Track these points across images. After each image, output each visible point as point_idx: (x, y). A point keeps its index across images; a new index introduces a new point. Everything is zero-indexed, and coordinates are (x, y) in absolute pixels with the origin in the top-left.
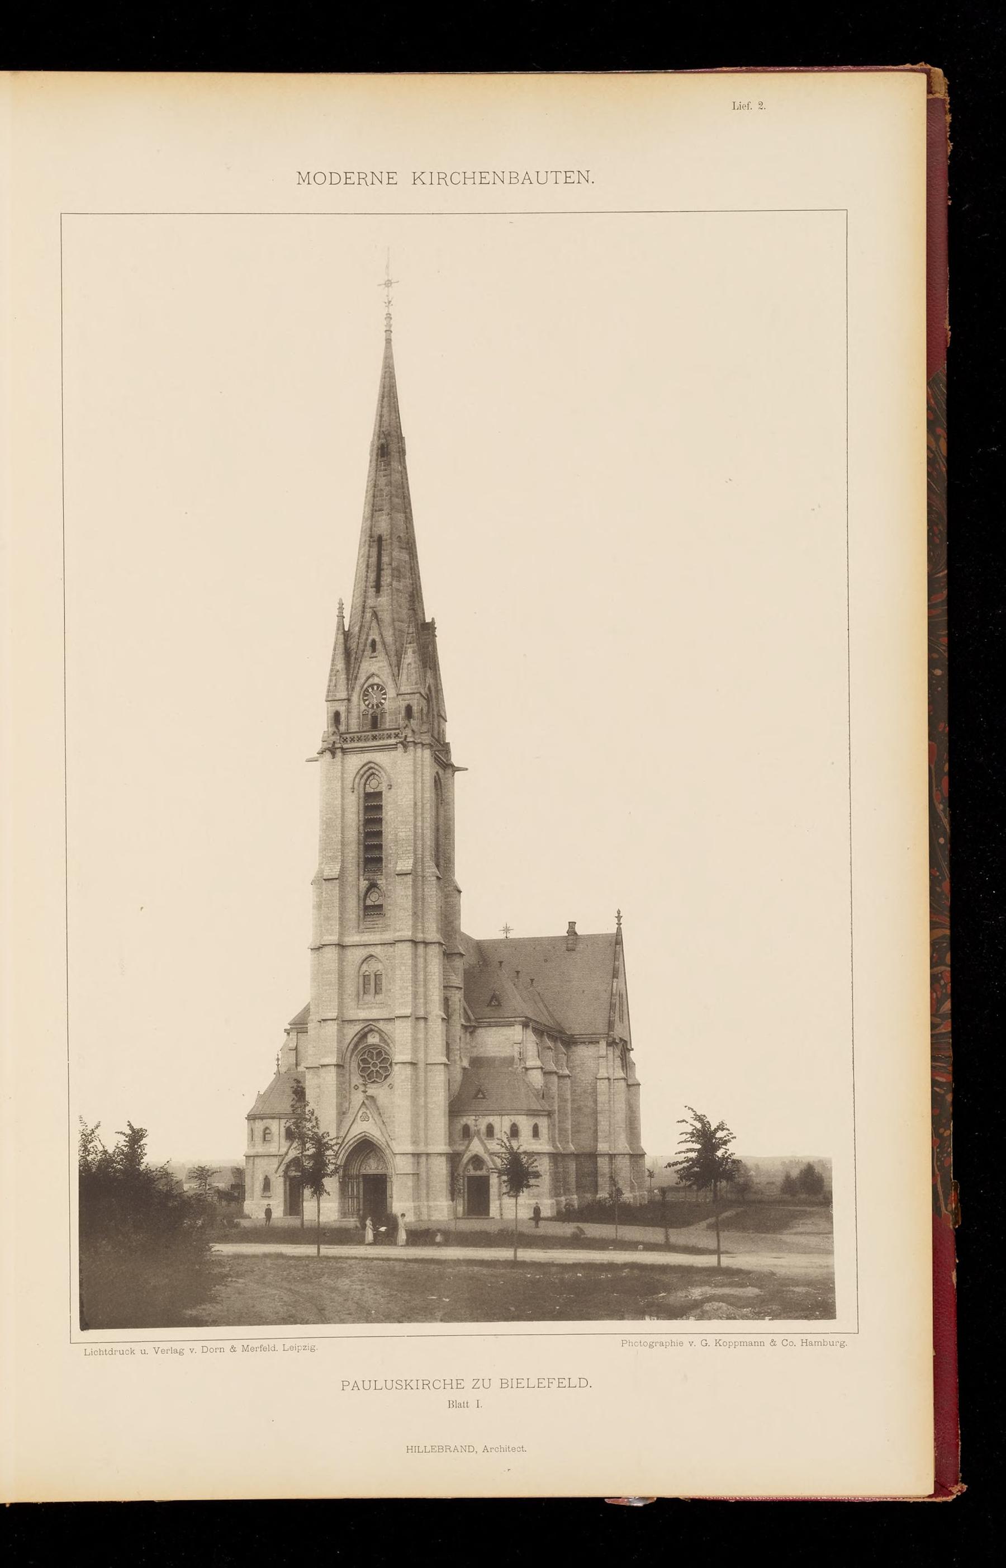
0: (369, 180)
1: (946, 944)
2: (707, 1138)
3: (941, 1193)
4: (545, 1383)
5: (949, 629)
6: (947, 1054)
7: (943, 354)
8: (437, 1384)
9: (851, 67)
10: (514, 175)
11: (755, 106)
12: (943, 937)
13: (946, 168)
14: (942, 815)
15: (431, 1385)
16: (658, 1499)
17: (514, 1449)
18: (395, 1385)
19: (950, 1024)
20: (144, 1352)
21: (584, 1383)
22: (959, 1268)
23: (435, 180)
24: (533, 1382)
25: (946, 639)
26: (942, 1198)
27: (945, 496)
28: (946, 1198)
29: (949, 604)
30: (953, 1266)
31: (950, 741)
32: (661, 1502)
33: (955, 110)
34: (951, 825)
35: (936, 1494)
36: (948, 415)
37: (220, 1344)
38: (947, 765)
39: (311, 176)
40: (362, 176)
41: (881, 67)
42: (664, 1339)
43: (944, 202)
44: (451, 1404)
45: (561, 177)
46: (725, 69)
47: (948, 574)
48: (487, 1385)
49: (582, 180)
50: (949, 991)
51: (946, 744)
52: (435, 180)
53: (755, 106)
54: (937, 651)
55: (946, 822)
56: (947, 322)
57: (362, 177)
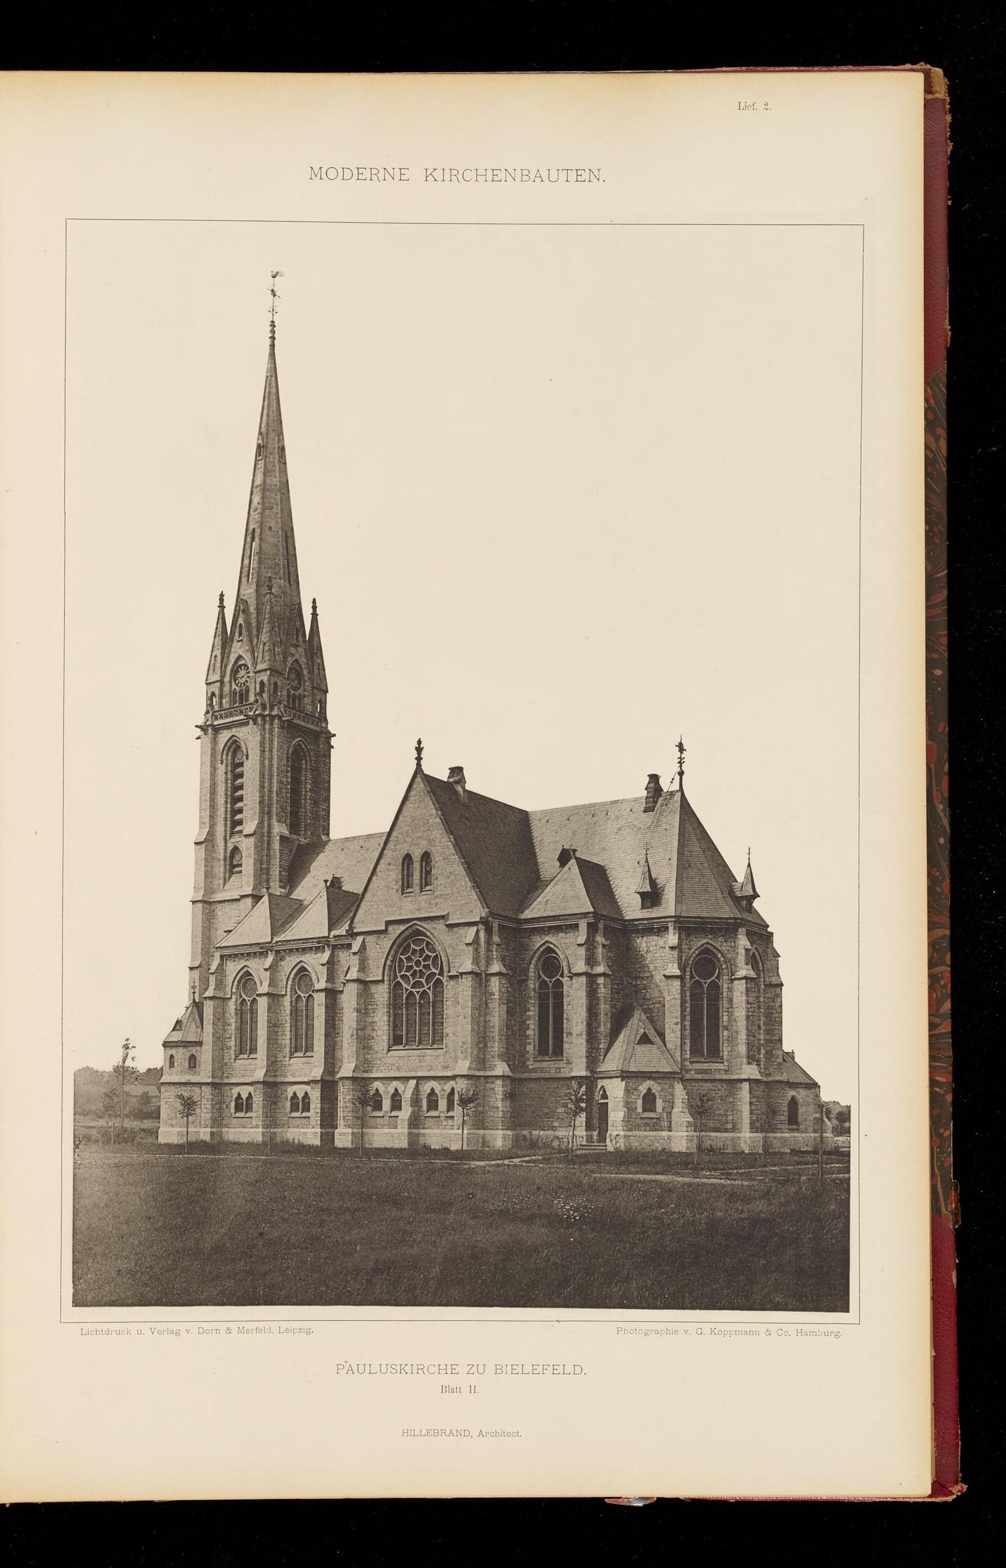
0: (381, 176)
1: (946, 944)
2: (457, 771)
3: (941, 1193)
4: (540, 1369)
6: (948, 1054)
7: (943, 354)
8: (432, 1369)
9: (851, 67)
10: (525, 173)
11: (760, 106)
13: (946, 168)
14: (942, 814)
15: (425, 1370)
16: (658, 1499)
17: (509, 1434)
20: (140, 1332)
21: (578, 1369)
23: (447, 177)
25: (946, 639)
26: (942, 1198)
27: (945, 496)
28: (946, 1199)
30: (952, 1266)
31: (950, 741)
32: (661, 1500)
33: (955, 109)
34: (951, 825)
35: (935, 1492)
36: (948, 415)
37: (215, 1326)
38: (947, 765)
39: (324, 171)
41: (882, 67)
42: (660, 1327)
43: (943, 201)
44: (444, 1389)
45: (572, 175)
46: (725, 69)
47: (948, 574)
48: (481, 1370)
50: (949, 991)
51: (946, 744)
52: (447, 177)
53: (760, 106)
54: (937, 651)
55: (946, 822)
56: (947, 322)
57: (374, 173)
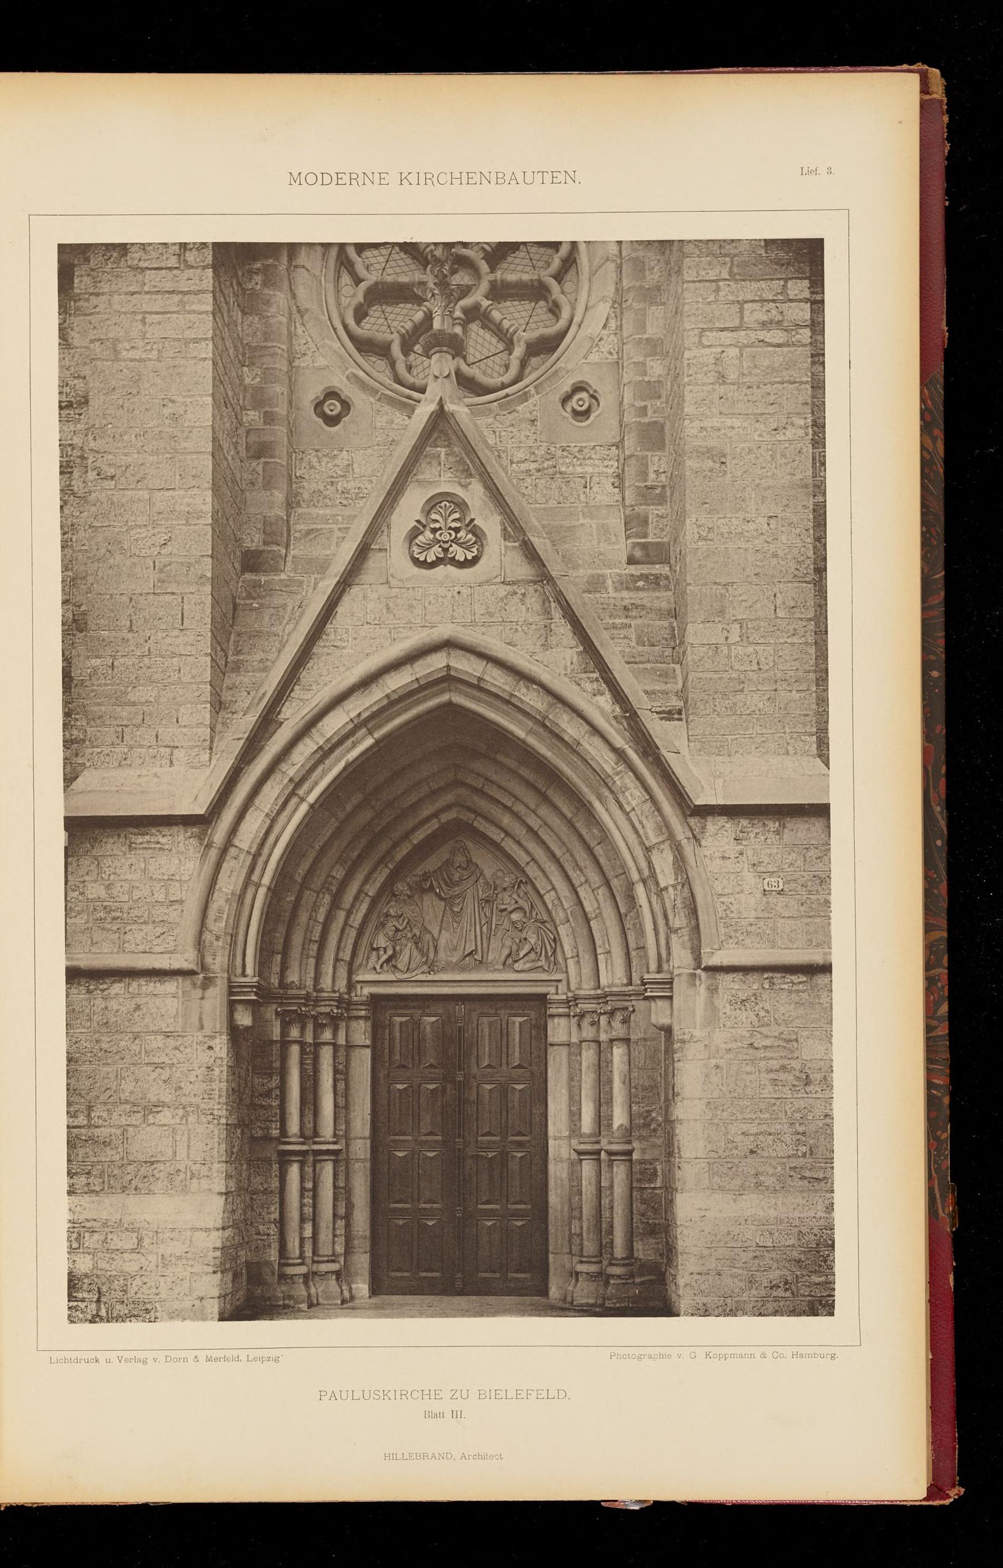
4: (524, 1394)
5: (947, 631)
9: (848, 68)
12: (940, 939)
14: (939, 817)
16: (655, 1502)
18: (372, 1395)
19: (947, 1026)
21: (562, 1394)
22: (957, 1271)
23: (422, 181)
24: (511, 1394)
27: (942, 497)
28: (943, 1201)
29: (946, 606)
30: (950, 1268)
32: (657, 1504)
33: (952, 109)
34: (948, 827)
39: (303, 176)
40: (354, 176)
41: (878, 68)
43: (939, 202)
44: (429, 1415)
45: (548, 178)
46: (721, 69)
48: (465, 1396)
49: (569, 180)
50: (946, 994)
51: (943, 746)
52: (422, 181)
54: (934, 653)
55: (943, 824)
56: (944, 323)
